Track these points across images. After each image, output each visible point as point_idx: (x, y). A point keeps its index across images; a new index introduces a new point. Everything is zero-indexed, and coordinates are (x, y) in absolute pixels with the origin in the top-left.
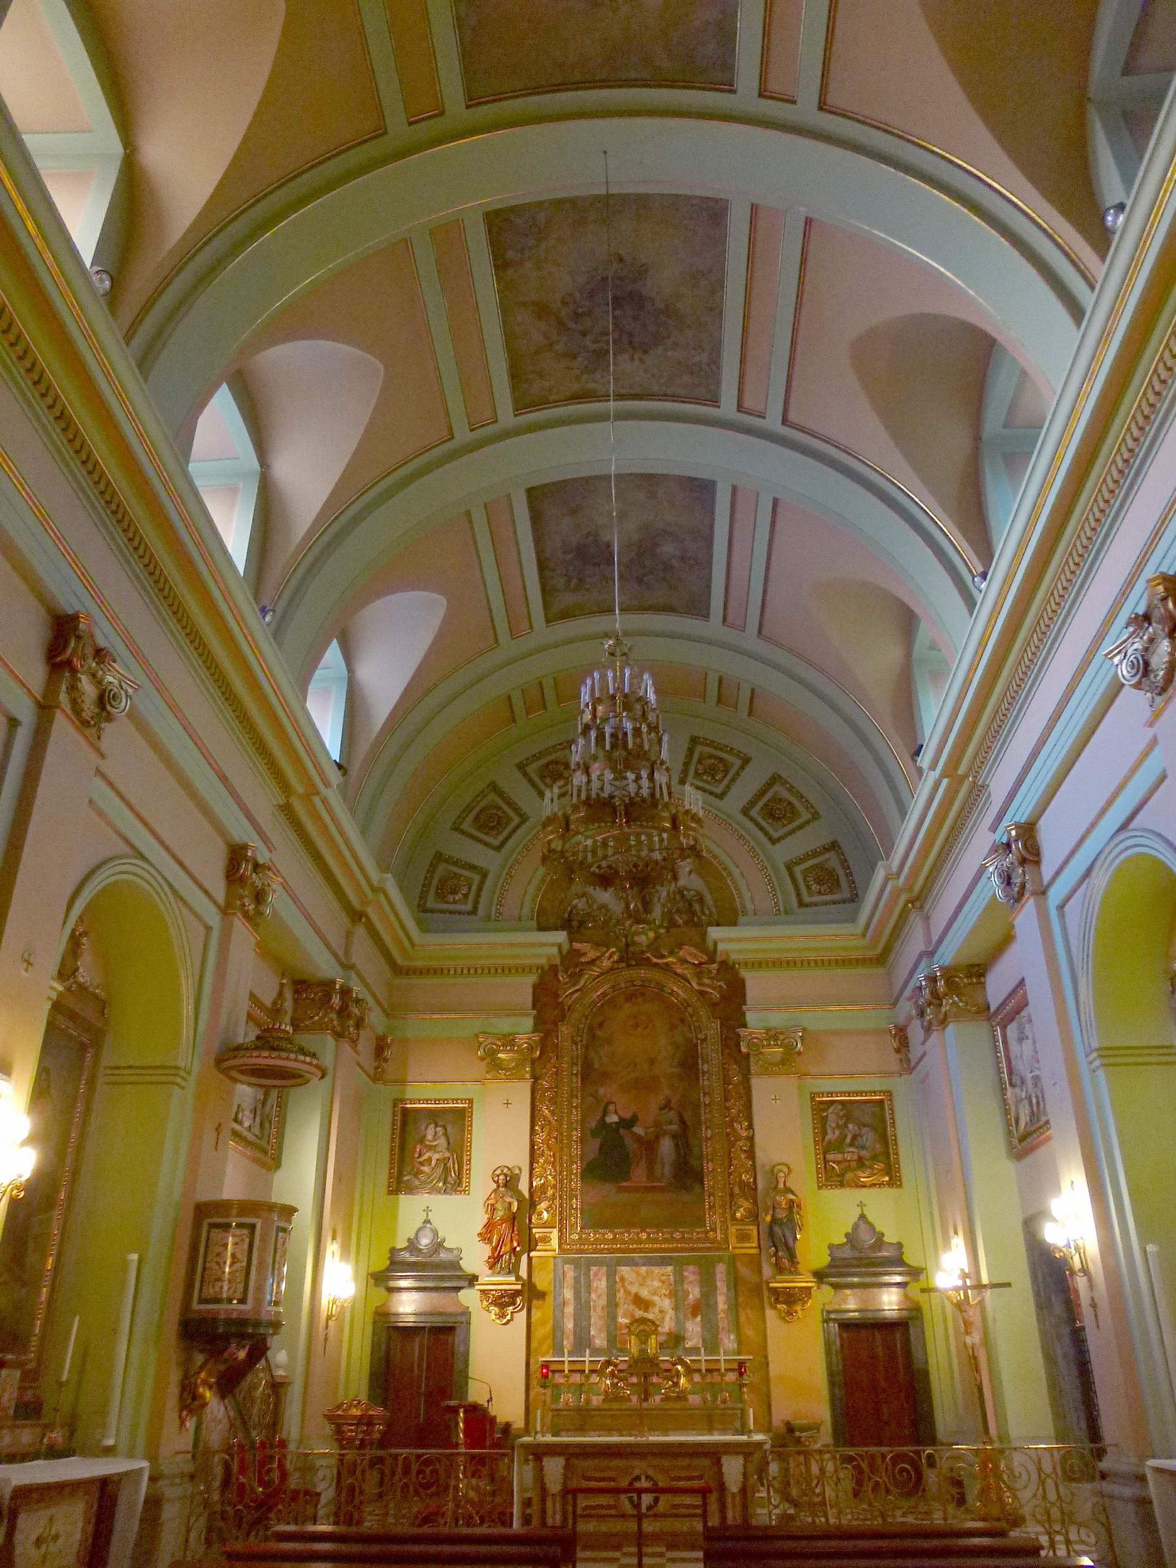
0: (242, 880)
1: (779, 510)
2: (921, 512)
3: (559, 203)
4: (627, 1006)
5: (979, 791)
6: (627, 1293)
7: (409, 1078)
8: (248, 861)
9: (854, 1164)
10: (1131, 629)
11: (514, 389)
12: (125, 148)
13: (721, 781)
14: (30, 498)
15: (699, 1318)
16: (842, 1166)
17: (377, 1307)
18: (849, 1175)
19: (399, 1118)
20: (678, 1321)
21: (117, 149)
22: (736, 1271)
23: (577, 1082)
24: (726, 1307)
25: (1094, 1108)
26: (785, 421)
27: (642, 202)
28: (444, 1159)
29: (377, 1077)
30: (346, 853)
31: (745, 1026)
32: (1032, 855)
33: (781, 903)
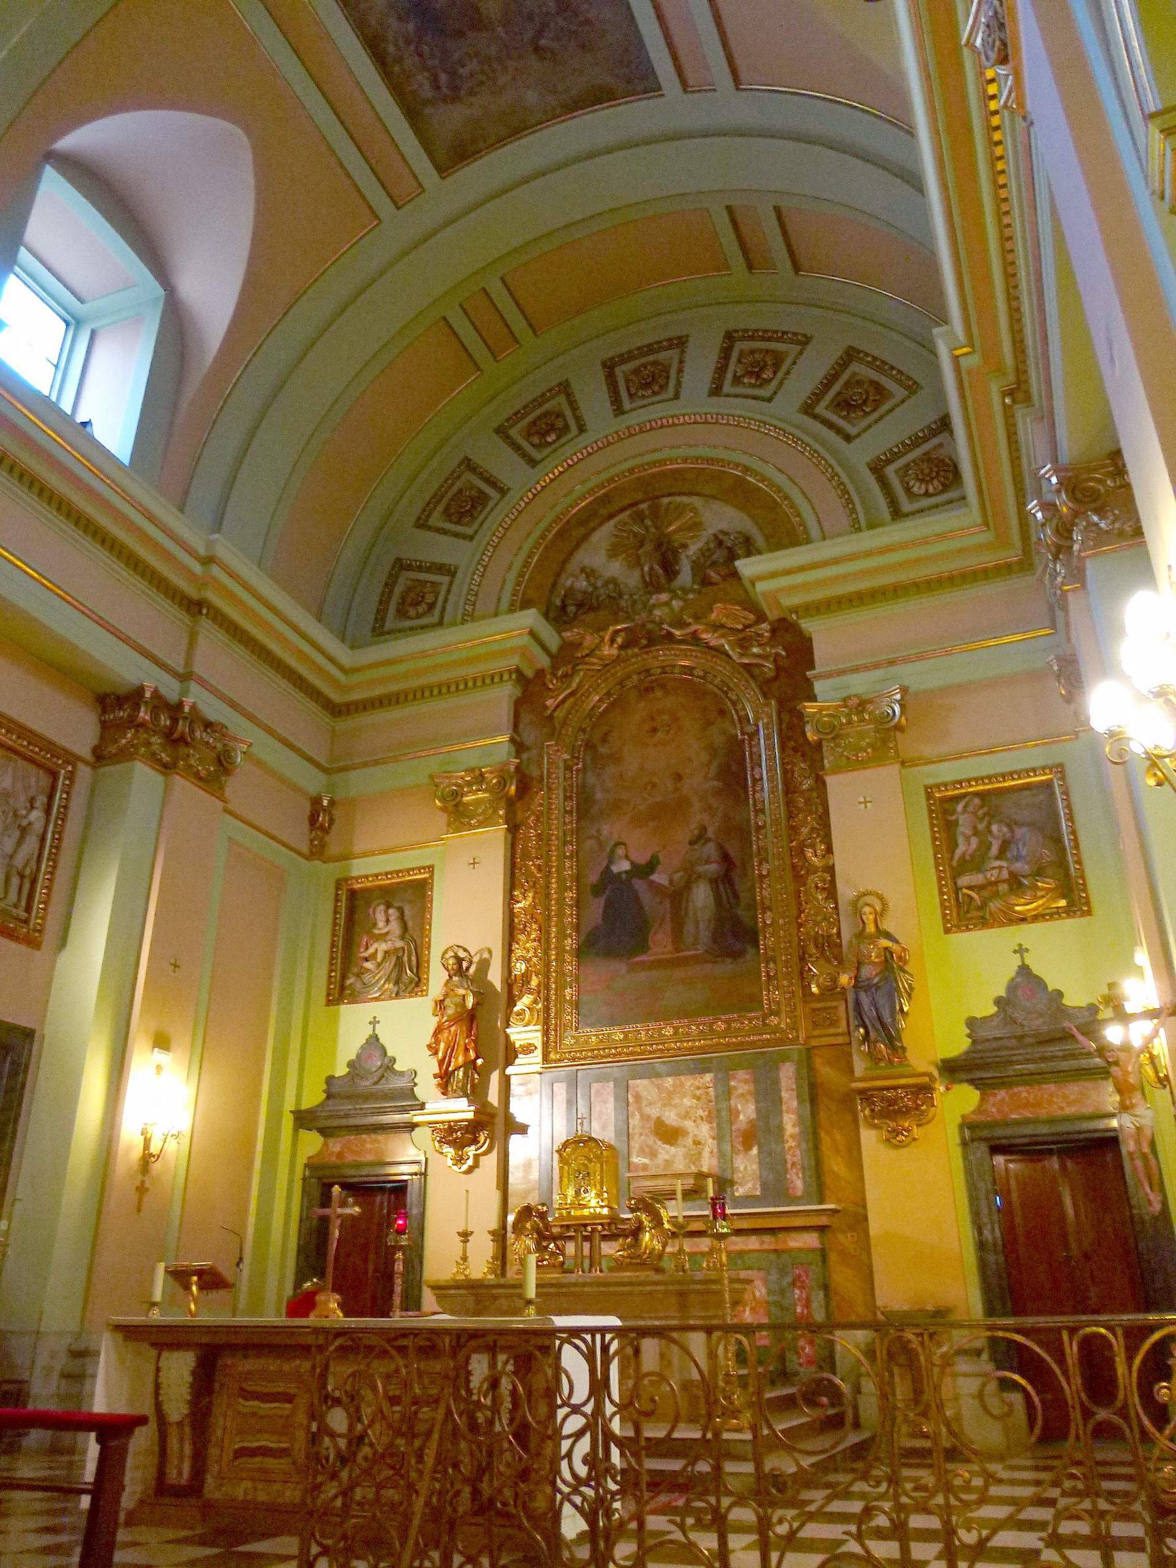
4: (642, 705)
6: (645, 1118)
7: (357, 849)
9: (1003, 888)
13: (770, 381)
15: (755, 1151)
16: (986, 893)
17: (309, 1158)
18: (995, 905)
19: (343, 904)
20: (721, 1155)
22: (811, 1068)
23: (572, 822)
24: (797, 1130)
25: (1023, 273)
28: (396, 950)
29: (317, 852)
31: (813, 698)
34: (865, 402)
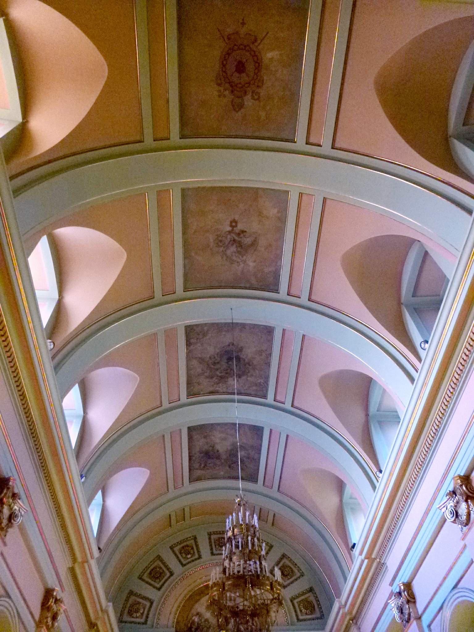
0: (49, 609)
1: (289, 439)
2: (348, 443)
3: (213, 324)
5: (381, 566)
8: (53, 598)
10: (448, 497)
11: (188, 388)
12: (59, 297)
14: (4, 429)
21: (57, 297)
26: (292, 406)
27: (243, 326)
30: (94, 593)
32: (412, 599)
33: (289, 619)
34: (288, 575)
